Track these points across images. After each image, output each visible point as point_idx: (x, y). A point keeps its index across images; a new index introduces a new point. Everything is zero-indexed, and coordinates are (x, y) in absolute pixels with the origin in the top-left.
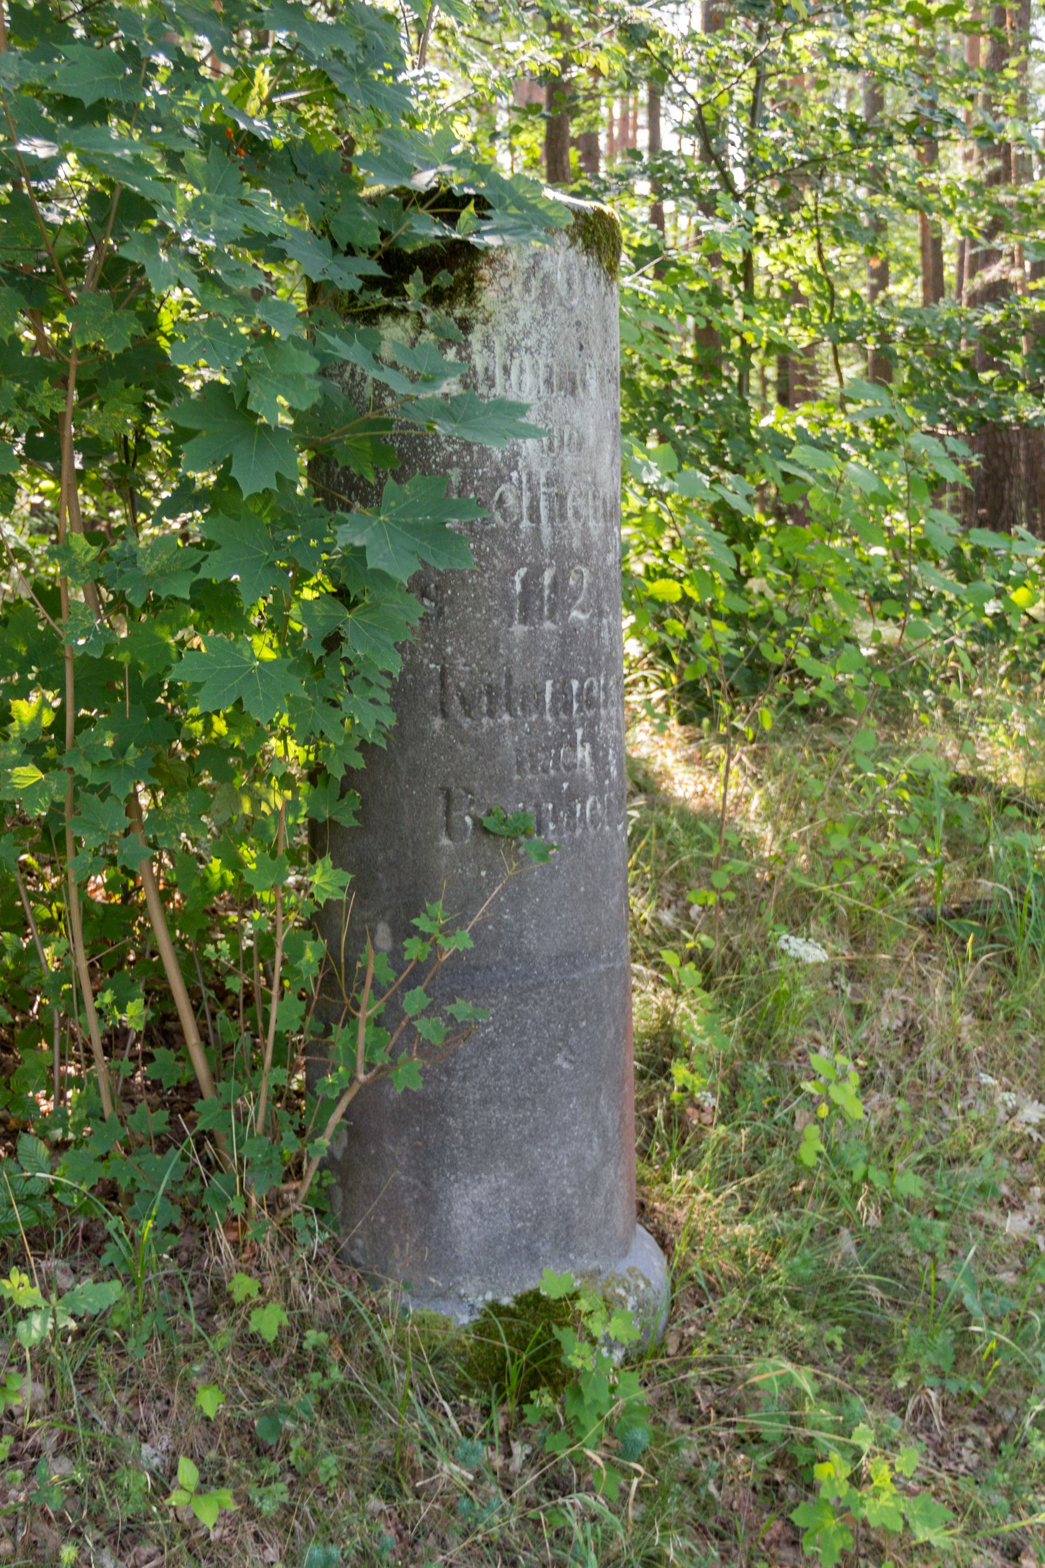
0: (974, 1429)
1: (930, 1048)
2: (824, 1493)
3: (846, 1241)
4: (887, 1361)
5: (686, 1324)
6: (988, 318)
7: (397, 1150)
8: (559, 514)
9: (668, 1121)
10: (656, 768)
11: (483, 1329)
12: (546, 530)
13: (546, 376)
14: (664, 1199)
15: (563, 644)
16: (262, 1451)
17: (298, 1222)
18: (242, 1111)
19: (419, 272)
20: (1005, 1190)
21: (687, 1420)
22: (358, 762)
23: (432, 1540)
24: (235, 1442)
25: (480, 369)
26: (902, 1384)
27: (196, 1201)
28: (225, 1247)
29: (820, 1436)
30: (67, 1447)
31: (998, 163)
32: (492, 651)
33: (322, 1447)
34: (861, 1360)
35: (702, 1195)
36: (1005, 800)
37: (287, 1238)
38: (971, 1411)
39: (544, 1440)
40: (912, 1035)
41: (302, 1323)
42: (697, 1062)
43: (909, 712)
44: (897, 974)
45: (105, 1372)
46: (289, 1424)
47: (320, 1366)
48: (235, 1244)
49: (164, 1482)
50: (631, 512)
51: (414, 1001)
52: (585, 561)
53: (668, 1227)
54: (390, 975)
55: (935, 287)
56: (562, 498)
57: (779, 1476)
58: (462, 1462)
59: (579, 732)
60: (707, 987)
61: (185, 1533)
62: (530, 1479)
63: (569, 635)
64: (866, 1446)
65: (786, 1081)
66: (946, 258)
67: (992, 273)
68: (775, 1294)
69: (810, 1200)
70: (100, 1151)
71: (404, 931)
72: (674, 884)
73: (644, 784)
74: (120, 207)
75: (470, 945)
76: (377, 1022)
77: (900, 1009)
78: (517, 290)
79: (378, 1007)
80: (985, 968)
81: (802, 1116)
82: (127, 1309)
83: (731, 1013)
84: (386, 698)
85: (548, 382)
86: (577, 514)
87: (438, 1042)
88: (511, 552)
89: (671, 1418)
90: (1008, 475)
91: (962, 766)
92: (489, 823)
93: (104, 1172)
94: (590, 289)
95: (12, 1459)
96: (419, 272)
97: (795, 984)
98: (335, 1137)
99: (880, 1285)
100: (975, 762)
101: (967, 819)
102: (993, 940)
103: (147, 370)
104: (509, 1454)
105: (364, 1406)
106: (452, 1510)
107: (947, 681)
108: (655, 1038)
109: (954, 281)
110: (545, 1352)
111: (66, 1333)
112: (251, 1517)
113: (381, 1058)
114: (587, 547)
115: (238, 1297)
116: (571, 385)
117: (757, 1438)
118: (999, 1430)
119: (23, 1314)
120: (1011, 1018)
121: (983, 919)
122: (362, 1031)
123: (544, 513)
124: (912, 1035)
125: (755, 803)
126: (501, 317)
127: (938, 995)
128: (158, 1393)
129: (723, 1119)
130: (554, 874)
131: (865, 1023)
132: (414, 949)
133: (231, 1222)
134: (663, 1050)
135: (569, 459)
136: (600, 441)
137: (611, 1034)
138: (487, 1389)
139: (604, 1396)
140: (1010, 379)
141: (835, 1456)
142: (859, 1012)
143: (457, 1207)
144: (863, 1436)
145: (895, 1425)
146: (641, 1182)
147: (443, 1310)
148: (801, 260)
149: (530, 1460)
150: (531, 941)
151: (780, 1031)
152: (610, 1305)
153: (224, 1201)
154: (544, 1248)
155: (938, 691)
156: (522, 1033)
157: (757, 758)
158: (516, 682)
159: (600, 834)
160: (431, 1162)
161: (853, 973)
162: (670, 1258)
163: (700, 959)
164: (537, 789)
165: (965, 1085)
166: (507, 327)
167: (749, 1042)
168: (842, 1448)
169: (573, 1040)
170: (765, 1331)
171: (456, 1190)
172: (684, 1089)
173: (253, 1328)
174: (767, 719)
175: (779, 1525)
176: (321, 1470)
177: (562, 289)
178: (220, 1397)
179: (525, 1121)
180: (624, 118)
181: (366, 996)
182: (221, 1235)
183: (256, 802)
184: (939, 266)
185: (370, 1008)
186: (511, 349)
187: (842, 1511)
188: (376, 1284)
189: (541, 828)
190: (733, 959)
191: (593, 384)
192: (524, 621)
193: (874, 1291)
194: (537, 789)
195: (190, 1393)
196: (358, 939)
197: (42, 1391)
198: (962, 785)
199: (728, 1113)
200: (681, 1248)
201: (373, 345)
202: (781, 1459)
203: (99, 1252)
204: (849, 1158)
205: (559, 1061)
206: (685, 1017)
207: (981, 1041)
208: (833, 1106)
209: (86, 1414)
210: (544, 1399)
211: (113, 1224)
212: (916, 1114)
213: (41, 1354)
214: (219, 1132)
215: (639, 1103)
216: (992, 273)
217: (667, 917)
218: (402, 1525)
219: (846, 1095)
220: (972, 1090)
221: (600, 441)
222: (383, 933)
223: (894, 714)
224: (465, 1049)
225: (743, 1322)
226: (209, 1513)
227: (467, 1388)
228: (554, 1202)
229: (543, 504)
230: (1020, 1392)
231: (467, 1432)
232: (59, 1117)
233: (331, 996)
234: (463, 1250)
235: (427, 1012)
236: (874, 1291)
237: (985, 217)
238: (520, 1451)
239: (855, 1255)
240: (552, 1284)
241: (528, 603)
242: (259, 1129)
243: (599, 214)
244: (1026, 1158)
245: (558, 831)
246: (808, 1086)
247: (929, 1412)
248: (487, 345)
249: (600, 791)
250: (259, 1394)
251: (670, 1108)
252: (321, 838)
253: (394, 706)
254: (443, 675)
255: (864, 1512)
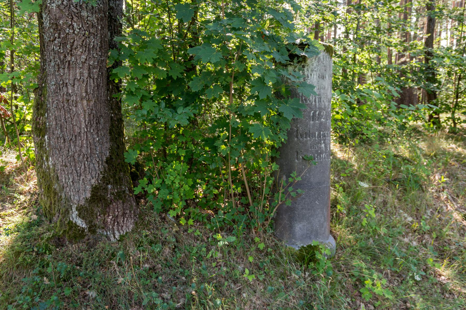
0: (397, 278)
1: (389, 205)
2: (367, 287)
3: (371, 240)
4: (379, 264)
5: (339, 253)
6: (403, 67)
7: (285, 217)
8: (320, 101)
9: (336, 216)
10: (334, 152)
11: (301, 250)
12: (317, 104)
13: (318, 77)
14: (335, 230)
15: (320, 125)
16: (260, 269)
17: (267, 229)
18: (257, 209)
19: (296, 58)
20: (404, 233)
21: (339, 271)
22: (281, 145)
23: (291, 288)
24: (255, 267)
25: (306, 74)
26: (382, 268)
27: (249, 224)
28: (254, 232)
29: (366, 276)
30: (226, 265)
31: (405, 38)
32: (307, 126)
33: (271, 269)
34: (374, 263)
35: (343, 230)
36: (404, 159)
37: (265, 232)
38: (396, 275)
39: (312, 272)
40: (385, 203)
41: (267, 247)
42: (342, 205)
43: (385, 142)
44: (382, 191)
45: (233, 253)
46: (265, 264)
47: (271, 255)
48: (256, 232)
49: (243, 272)
50: (333, 103)
51: (290, 189)
52: (324, 110)
53: (336, 235)
54: (285, 184)
55: (390, 62)
56: (321, 98)
57: (357, 283)
58: (297, 274)
59: (322, 142)
60: (344, 191)
61: (246, 282)
62: (309, 278)
63: (321, 123)
64: (376, 278)
65: (360, 210)
66: (393, 58)
67: (403, 60)
68: (357, 249)
69: (364, 232)
70: (232, 214)
71: (288, 176)
72: (338, 173)
73: (332, 154)
74: (241, 47)
75: (301, 179)
76: (283, 193)
77: (383, 198)
78: (313, 60)
79: (283, 190)
80: (400, 191)
81: (362, 217)
82: (237, 242)
83: (349, 197)
84: (286, 134)
85: (319, 77)
86: (323, 101)
87: (294, 197)
88: (311, 108)
89: (336, 271)
90: (405, 99)
91: (395, 153)
92: (305, 158)
93: (232, 217)
94: (327, 60)
95: (216, 266)
96: (296, 58)
97: (361, 192)
98: (274, 214)
99: (378, 249)
100: (398, 152)
101: (397, 162)
102: (402, 185)
103: (245, 75)
104: (305, 274)
105: (279, 263)
106: (295, 283)
107: (393, 137)
108: (334, 200)
109: (394, 62)
110: (312, 256)
111: (226, 245)
112: (258, 281)
113: (284, 200)
114: (325, 107)
115: (256, 241)
116: (323, 77)
117: (353, 276)
118: (402, 279)
119: (219, 241)
120: (405, 201)
121: (400, 182)
122: (280, 194)
123: (317, 101)
124: (385, 203)
125: (353, 159)
126: (310, 65)
127: (390, 195)
128: (242, 257)
129: (347, 216)
130: (317, 168)
131: (375, 200)
132: (290, 180)
133: (255, 228)
134: (335, 203)
135: (322, 91)
136: (328, 88)
137: (326, 198)
138: (301, 262)
139: (324, 265)
140: (407, 79)
141: (369, 280)
142: (374, 198)
143: (297, 228)
144: (375, 276)
145: (381, 275)
146: (331, 227)
147: (293, 247)
148: (365, 57)
149: (309, 276)
150: (312, 180)
151: (358, 200)
152: (326, 248)
153: (254, 224)
154: (312, 237)
155: (391, 139)
156: (310, 197)
157: (354, 150)
158: (311, 132)
159: (325, 160)
160: (292, 219)
161: (373, 190)
162: (336, 241)
163: (343, 186)
164: (314, 152)
165: (395, 213)
166: (312, 67)
167: (352, 202)
168: (370, 278)
169: (319, 199)
170: (355, 256)
171: (296, 225)
172: (339, 210)
173: (259, 247)
174: (357, 141)
175: (357, 292)
176: (270, 273)
177: (322, 60)
178: (253, 259)
179: (310, 213)
180: (329, 34)
181: (281, 188)
182: (254, 231)
183: (263, 152)
184: (391, 59)
185: (282, 190)
186: (312, 71)
187: (370, 290)
188: (281, 241)
189: (314, 159)
190: (349, 187)
191: (327, 77)
192: (313, 121)
193: (377, 250)
194: (314, 152)
195: (247, 258)
196: (280, 178)
197: (221, 255)
198: (395, 156)
199: (348, 214)
200: (339, 239)
201: (287, 71)
202: (358, 280)
203: (232, 231)
204: (372, 225)
205: (316, 202)
206: (339, 197)
207: (399, 205)
208: (370, 215)
209: (229, 260)
210: (312, 264)
211: (235, 226)
212: (385, 218)
213: (222, 248)
214: (253, 212)
215: (331, 212)
216: (403, 60)
217: (336, 179)
218: (285, 285)
219: (372, 212)
220: (397, 214)
221: (328, 88)
222: (284, 177)
223: (382, 143)
224: (299, 199)
225: (350, 254)
226: (251, 278)
227: (297, 261)
228: (315, 228)
229: (317, 99)
230: (407, 272)
231: (297, 269)
232: (225, 207)
233: (274, 188)
234: (297, 236)
235: (293, 191)
236: (377, 250)
237: (402, 48)
238: (307, 273)
239: (373, 243)
240: (314, 243)
241: (313, 118)
242: (261, 211)
243: (329, 46)
244: (408, 228)
245: (318, 160)
246: (364, 211)
247: (388, 274)
248: (308, 70)
249: (326, 153)
250: (260, 259)
251: (336, 213)
252: (273, 159)
253: (288, 136)
254: (297, 130)
255: (375, 291)
